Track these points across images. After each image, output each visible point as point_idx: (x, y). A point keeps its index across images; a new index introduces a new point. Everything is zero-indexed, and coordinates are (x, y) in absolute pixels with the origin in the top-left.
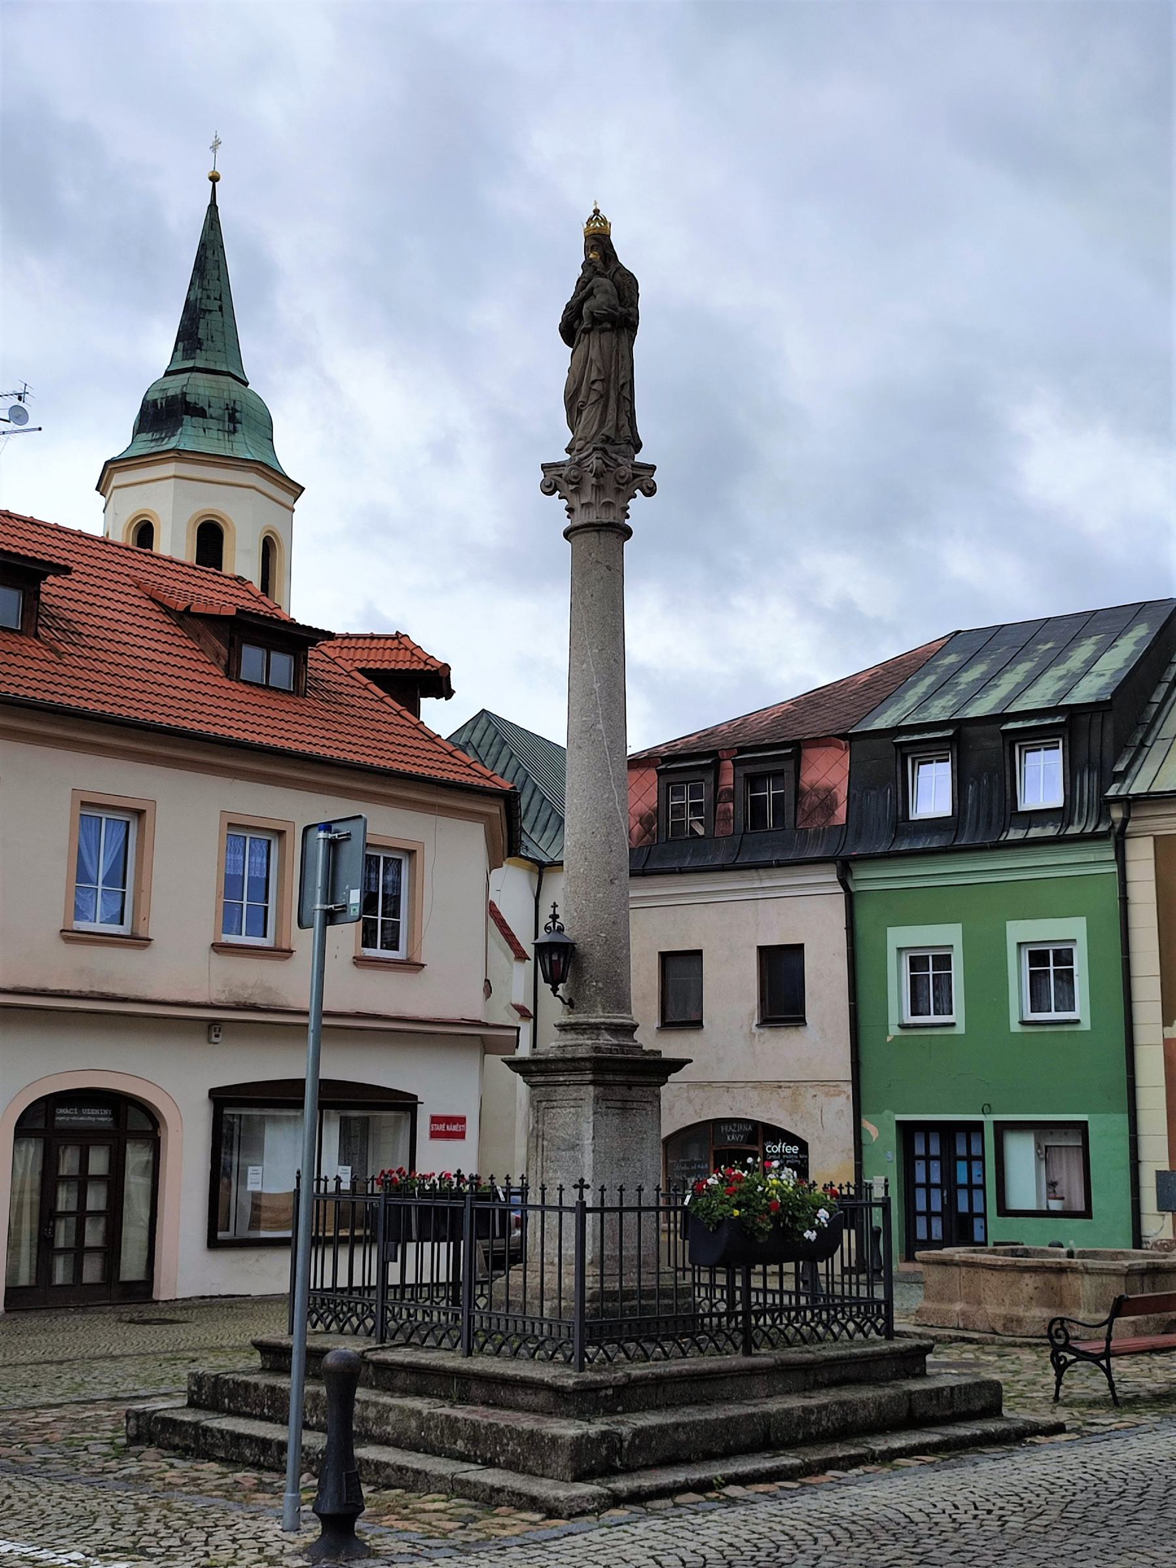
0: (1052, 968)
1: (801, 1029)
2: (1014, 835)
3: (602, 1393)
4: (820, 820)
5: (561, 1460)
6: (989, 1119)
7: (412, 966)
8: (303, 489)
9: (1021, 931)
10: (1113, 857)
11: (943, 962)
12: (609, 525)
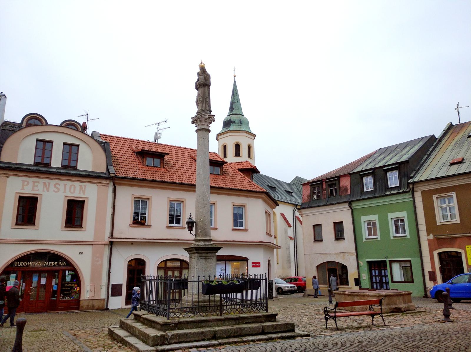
0: (372, 226)
1: (344, 241)
2: (388, 193)
3: (171, 325)
4: (344, 193)
5: (150, 342)
6: (388, 260)
7: (246, 230)
8: (256, 135)
9: (391, 215)
10: (411, 197)
11: (374, 223)
12: (203, 129)
